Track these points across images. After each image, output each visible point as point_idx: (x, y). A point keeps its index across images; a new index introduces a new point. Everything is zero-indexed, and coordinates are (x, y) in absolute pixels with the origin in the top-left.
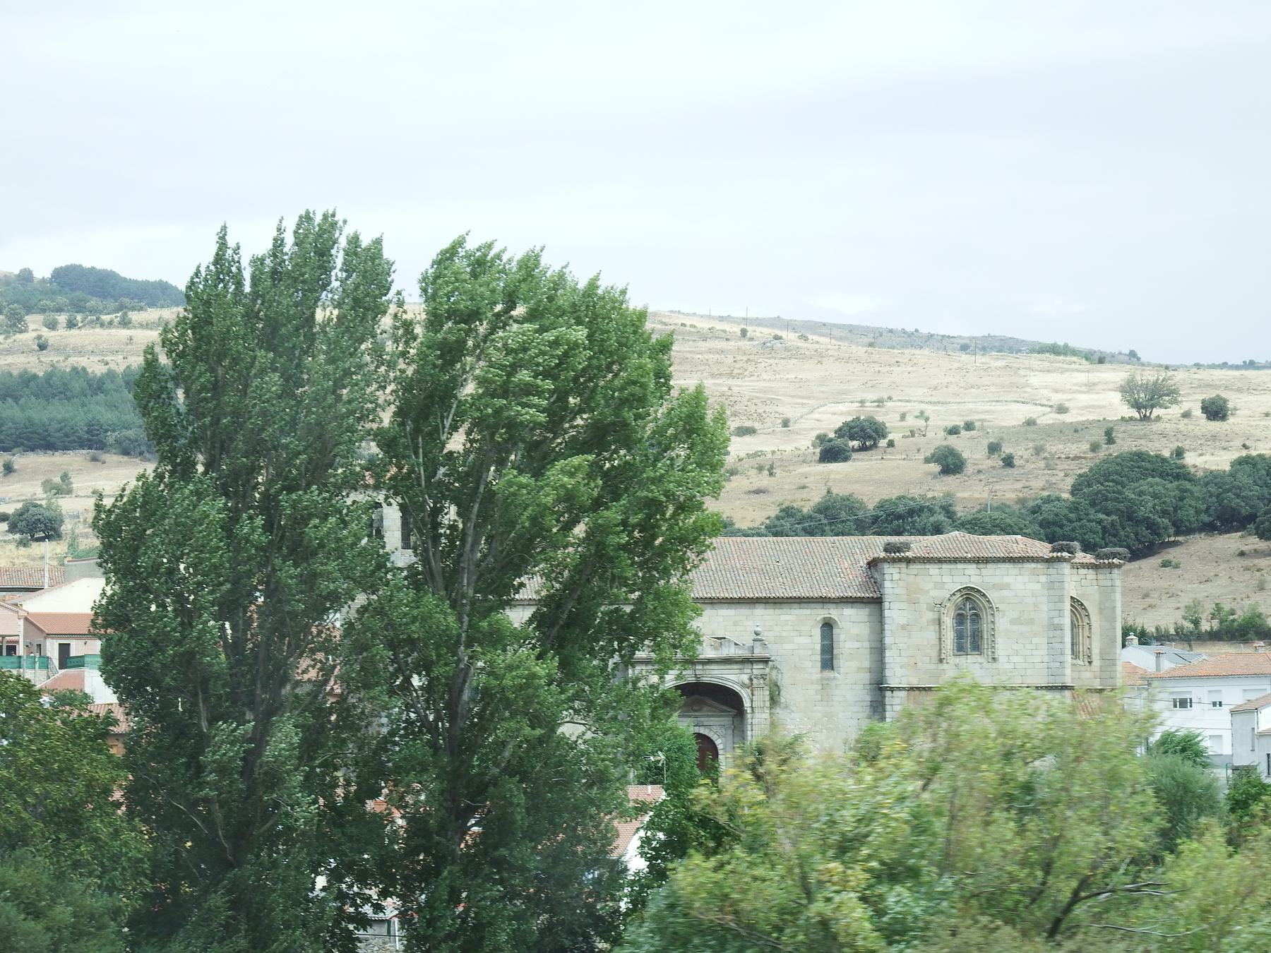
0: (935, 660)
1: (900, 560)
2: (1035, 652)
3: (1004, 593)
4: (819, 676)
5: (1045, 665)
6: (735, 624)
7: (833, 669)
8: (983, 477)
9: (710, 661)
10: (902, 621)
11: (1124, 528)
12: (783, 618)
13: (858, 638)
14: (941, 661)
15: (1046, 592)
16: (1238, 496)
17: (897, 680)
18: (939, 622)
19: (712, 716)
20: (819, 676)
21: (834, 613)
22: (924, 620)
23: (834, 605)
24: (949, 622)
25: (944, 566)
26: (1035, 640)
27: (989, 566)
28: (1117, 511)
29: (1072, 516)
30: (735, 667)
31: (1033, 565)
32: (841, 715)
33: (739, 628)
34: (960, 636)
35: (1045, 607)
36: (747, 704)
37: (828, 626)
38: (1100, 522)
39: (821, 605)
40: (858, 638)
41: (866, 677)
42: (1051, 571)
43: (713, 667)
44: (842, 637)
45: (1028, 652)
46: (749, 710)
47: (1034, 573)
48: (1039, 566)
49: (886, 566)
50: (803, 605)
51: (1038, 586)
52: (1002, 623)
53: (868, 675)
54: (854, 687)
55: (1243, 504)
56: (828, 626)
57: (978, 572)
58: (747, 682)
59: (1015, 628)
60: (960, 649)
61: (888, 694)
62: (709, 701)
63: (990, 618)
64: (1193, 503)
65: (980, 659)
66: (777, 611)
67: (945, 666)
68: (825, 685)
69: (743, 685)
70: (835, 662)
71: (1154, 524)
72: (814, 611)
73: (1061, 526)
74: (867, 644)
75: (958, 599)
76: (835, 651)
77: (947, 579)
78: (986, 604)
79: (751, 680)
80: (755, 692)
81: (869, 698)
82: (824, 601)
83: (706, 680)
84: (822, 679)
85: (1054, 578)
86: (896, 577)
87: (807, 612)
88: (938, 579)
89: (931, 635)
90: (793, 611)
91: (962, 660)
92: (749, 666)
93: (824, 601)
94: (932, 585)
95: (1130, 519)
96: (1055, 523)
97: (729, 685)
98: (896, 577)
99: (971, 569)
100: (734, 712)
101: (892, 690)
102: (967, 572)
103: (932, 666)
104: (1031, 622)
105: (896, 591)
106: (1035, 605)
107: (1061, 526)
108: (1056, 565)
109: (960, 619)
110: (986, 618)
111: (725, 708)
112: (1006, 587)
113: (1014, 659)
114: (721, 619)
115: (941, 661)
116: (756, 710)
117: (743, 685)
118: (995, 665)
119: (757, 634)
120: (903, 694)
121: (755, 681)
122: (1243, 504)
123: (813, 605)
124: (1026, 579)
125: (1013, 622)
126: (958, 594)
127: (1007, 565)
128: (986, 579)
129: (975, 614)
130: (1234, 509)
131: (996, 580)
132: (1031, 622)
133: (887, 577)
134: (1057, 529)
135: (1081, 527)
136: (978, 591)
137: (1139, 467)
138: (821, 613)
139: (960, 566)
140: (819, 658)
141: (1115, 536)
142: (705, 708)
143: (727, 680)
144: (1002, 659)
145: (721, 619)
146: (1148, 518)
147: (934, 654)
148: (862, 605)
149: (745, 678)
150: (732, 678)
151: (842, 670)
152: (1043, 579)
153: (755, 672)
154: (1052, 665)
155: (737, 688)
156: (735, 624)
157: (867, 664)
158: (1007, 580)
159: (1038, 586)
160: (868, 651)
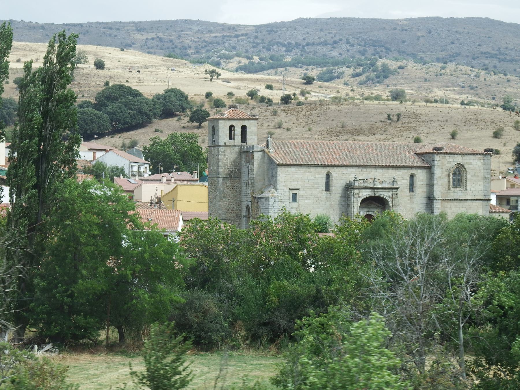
0: (447, 189)
1: (440, 153)
2: (479, 187)
3: (470, 166)
4: (409, 194)
5: (482, 192)
6: (383, 175)
7: (413, 192)
8: (260, 110)
9: (380, 188)
10: (440, 175)
11: (138, 116)
12: (398, 173)
13: (422, 181)
14: (449, 189)
15: (483, 166)
16: (171, 104)
17: (438, 196)
18: (449, 175)
19: (374, 208)
20: (409, 194)
21: (415, 171)
22: (444, 175)
23: (415, 169)
24: (451, 175)
25: (451, 156)
26: (479, 183)
27: (466, 156)
28: (135, 109)
29: (119, 111)
30: (387, 190)
31: (479, 156)
32: (416, 208)
33: (384, 176)
34: (454, 181)
35: (482, 171)
36: (390, 204)
37: (412, 176)
38: (129, 113)
39: (410, 169)
40: (422, 181)
41: (424, 195)
42: (485, 158)
43: (380, 190)
44: (417, 180)
45: (477, 187)
46: (391, 206)
47: (479, 159)
48: (481, 156)
49: (435, 155)
50: (405, 169)
51: (481, 164)
52: (469, 176)
53: (425, 194)
54: (421, 198)
55: (174, 108)
56: (412, 176)
57: (461, 158)
58: (391, 196)
59: (473, 178)
60: (454, 185)
61: (435, 201)
62: (374, 203)
63: (465, 175)
64: (159, 107)
65: (461, 189)
66: (396, 171)
67: (450, 191)
68: (411, 197)
69: (390, 197)
70: (414, 189)
71: (148, 115)
72: (408, 171)
73: (115, 115)
74: (425, 183)
75: (455, 167)
76: (414, 185)
77: (451, 160)
78: (464, 169)
79: (392, 195)
80: (394, 200)
81: (425, 202)
82: (412, 167)
83: (377, 195)
84: (410, 195)
85: (486, 161)
86: (438, 159)
87: (406, 171)
88: (448, 160)
89: (446, 180)
90: (401, 171)
91: (455, 189)
92: (392, 190)
93: (412, 167)
94: (446, 163)
95: (140, 112)
96: (113, 113)
97: (385, 197)
98: (438, 159)
99: (459, 157)
100: (382, 207)
101: (436, 200)
102: (458, 158)
103: (446, 191)
104: (478, 176)
105: (438, 164)
106: (480, 170)
107: (115, 115)
108: (487, 156)
109: (454, 174)
110: (463, 174)
111: (379, 205)
112: (471, 163)
113: (472, 189)
114: (378, 173)
115: (449, 189)
116: (394, 206)
117: (390, 197)
118: (466, 191)
119: (394, 179)
120: (440, 201)
121: (394, 196)
122: (174, 108)
123: (408, 169)
124: (477, 161)
125: (472, 176)
126: (455, 166)
127: (471, 156)
128: (464, 161)
129: (459, 173)
130: (170, 109)
131: (467, 161)
132: (478, 176)
133: (435, 159)
134: (114, 116)
135: (123, 115)
136: (462, 165)
137: (122, 91)
138: (410, 171)
139: (456, 156)
140: (409, 187)
141: (135, 119)
142: (372, 205)
143: (384, 195)
144: (468, 189)
145: (378, 173)
146: (146, 112)
147: (447, 187)
148: (424, 169)
149: (390, 195)
150: (386, 195)
151: (417, 192)
152: (482, 161)
153: (394, 192)
154: (485, 192)
155: (387, 198)
156: (383, 175)
157: (425, 190)
158: (471, 161)
159: (481, 164)
160: (425, 186)
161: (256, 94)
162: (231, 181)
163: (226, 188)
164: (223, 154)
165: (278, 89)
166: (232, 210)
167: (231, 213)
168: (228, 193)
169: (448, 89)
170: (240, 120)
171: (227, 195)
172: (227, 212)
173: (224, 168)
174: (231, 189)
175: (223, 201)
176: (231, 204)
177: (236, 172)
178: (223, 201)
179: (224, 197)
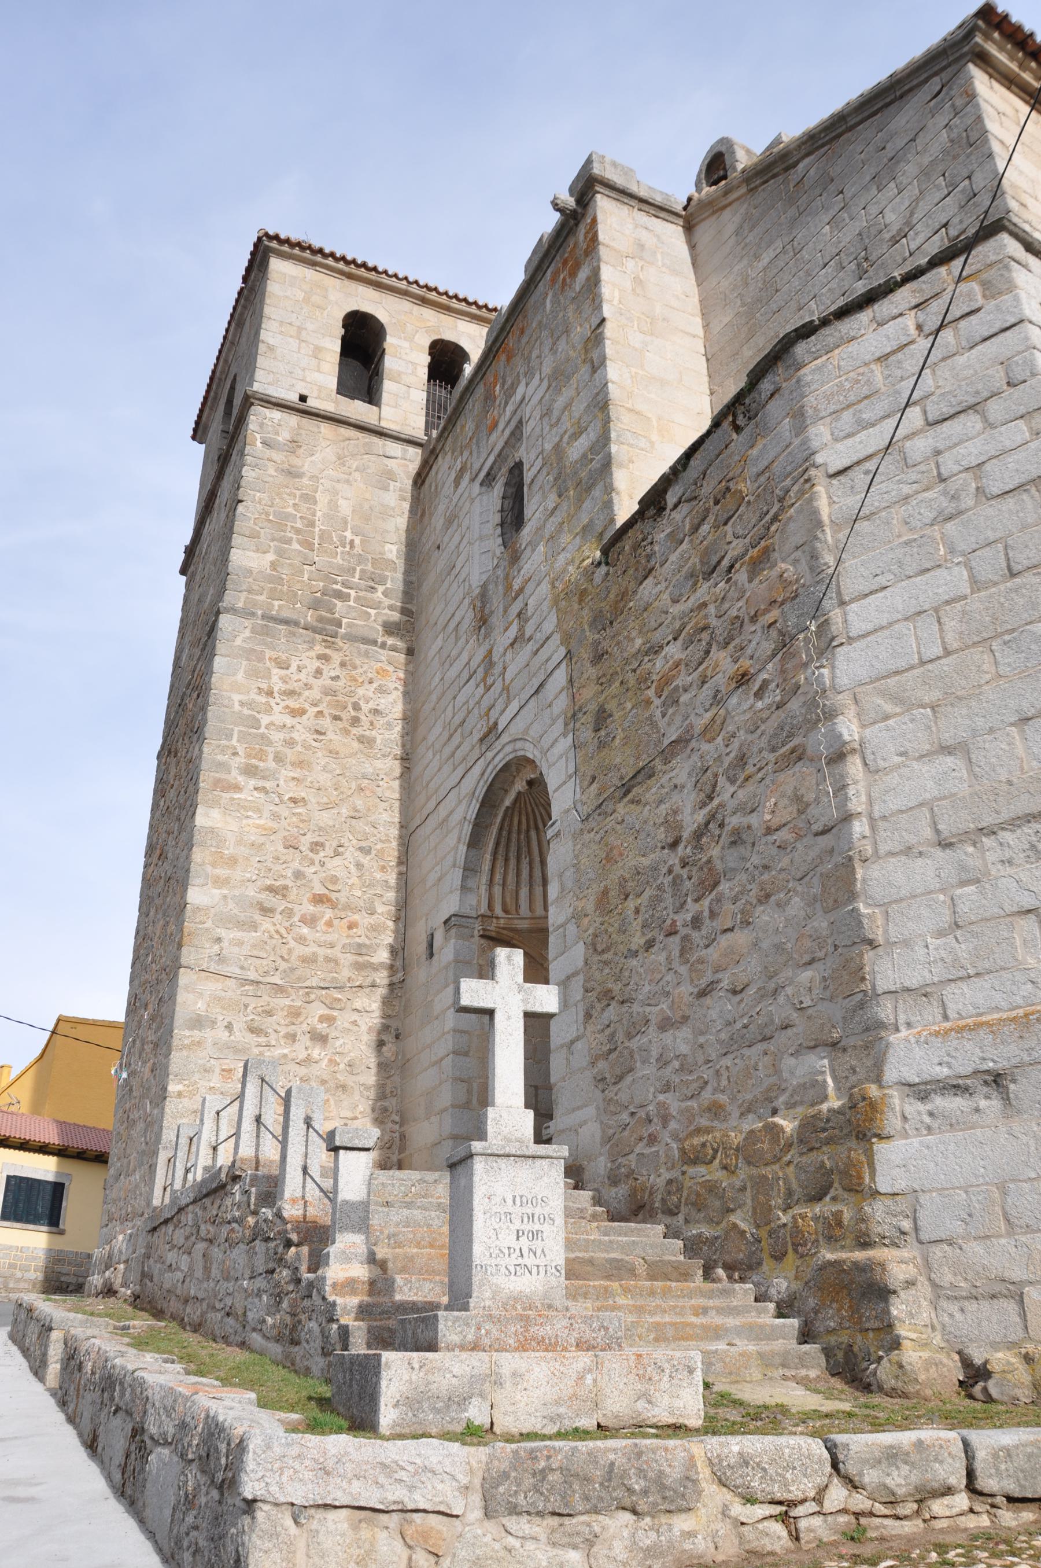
25: (281, 1119)
161: (259, 1400)
162: (324, 658)
163: (278, 705)
164: (278, 456)
165: (556, 740)
166: (318, 899)
167: (310, 921)
168: (290, 743)
169: (789, 1373)
170: (424, 301)
171: (279, 759)
172: (266, 911)
173: (280, 553)
174: (326, 723)
175: (242, 806)
176: (316, 847)
177: (377, 606)
178: (242, 806)
179: (250, 771)
